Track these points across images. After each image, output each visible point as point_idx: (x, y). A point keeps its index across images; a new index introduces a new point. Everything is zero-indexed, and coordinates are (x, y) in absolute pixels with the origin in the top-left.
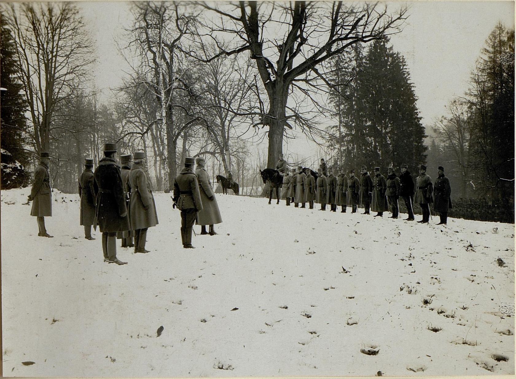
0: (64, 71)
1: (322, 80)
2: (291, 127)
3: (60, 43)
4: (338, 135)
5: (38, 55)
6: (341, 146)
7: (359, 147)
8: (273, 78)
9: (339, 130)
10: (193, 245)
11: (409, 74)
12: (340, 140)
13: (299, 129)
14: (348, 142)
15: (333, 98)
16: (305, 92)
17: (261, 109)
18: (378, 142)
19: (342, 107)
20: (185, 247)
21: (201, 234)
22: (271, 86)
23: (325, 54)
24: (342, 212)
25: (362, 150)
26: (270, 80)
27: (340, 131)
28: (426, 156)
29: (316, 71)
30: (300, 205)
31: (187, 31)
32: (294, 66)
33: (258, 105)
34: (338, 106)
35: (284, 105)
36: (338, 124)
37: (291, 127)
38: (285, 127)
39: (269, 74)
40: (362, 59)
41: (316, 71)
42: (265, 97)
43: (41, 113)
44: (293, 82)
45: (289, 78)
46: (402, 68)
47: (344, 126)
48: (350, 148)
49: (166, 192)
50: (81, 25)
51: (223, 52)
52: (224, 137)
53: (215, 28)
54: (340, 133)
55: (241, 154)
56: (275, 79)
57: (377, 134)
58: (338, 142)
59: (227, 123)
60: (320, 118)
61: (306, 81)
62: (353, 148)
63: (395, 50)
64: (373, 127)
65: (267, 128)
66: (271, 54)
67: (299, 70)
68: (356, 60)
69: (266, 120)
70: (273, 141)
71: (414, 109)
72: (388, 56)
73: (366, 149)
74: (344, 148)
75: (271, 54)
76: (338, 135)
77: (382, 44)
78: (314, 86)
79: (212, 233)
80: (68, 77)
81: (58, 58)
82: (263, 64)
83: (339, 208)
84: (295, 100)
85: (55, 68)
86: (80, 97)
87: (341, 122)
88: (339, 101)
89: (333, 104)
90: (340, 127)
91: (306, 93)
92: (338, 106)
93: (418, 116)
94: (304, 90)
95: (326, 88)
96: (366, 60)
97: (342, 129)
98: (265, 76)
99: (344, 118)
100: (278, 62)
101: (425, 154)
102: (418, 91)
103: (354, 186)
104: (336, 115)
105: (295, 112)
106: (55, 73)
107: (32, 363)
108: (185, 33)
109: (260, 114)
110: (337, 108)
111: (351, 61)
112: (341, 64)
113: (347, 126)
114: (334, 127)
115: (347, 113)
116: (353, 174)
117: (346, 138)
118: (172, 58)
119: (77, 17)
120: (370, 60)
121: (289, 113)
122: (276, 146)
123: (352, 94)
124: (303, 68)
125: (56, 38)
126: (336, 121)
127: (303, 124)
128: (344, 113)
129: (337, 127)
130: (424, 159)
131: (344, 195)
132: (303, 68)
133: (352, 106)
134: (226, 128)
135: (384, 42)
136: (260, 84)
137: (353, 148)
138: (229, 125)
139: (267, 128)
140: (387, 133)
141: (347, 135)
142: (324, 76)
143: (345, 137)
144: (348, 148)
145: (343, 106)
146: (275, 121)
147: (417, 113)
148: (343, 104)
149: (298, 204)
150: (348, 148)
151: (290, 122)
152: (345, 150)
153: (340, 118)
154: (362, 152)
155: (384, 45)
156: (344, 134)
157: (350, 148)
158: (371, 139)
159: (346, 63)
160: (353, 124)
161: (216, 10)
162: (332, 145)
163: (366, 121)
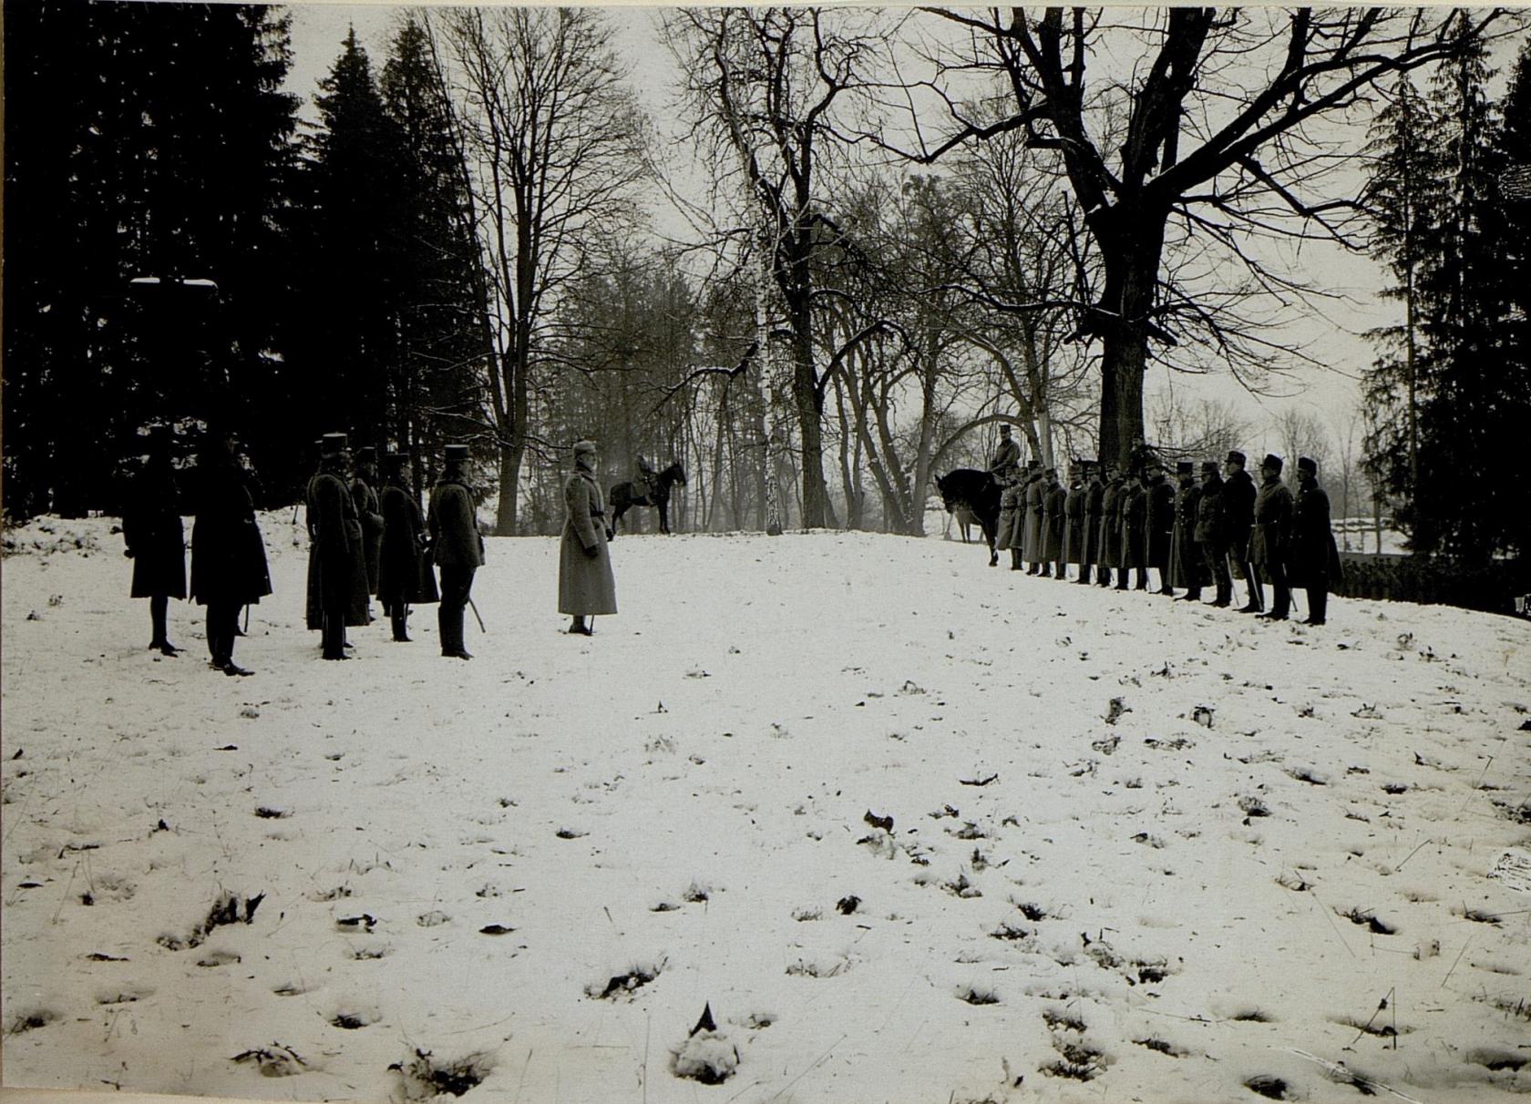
0: (561, 207)
1: (1275, 194)
3: (556, 130)
5: (495, 165)
10: (468, 648)
12: (1414, 371)
14: (1444, 377)
15: (1390, 240)
16: (1224, 234)
20: (446, 653)
21: (571, 631)
26: (1104, 202)
27: (1412, 345)
31: (851, 81)
36: (1404, 322)
38: (1151, 343)
41: (1255, 168)
43: (506, 320)
47: (1424, 327)
49: (770, 533)
50: (609, 76)
51: (971, 130)
53: (947, 59)
54: (1413, 352)
61: (1217, 201)
65: (1098, 347)
66: (1104, 125)
68: (1463, 116)
70: (1114, 381)
75: (1104, 125)
76: (1403, 356)
80: (576, 221)
81: (549, 173)
82: (1083, 163)
85: (542, 198)
86: (626, 272)
87: (1414, 318)
90: (1411, 332)
94: (1216, 227)
95: (725, 268)
97: (1421, 339)
104: (1399, 293)
106: (541, 210)
108: (844, 86)
111: (1445, 119)
114: (1390, 332)
115: (1435, 284)
116: (1137, 481)
118: (805, 159)
119: (595, 56)
122: (1122, 396)
124: (1209, 161)
125: (543, 116)
126: (1397, 312)
129: (1400, 330)
131: (1115, 541)
132: (1209, 161)
142: (1280, 180)
150: (1442, 397)
153: (1411, 303)
156: (1425, 353)
161: (940, 12)
162: (1386, 389)
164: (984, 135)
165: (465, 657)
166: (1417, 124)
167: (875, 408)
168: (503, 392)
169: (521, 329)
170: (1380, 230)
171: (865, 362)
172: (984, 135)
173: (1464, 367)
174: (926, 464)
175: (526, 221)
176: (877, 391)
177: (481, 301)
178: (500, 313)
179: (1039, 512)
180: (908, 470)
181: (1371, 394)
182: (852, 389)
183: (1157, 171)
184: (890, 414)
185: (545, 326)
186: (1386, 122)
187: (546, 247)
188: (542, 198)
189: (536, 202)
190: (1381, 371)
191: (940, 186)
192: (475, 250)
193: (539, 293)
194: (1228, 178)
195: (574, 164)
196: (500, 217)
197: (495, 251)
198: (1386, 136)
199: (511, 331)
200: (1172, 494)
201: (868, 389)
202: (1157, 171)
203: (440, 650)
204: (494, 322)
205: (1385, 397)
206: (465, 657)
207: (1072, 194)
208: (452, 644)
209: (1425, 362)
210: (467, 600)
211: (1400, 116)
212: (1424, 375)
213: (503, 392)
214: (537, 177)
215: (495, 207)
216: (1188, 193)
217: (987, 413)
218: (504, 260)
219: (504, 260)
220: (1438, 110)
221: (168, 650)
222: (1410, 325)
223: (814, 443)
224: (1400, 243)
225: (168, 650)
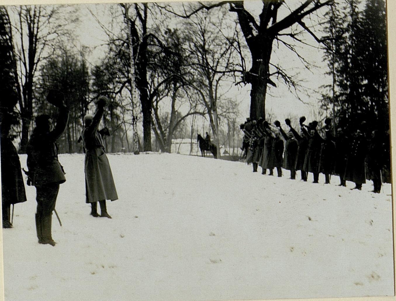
2: (274, 85)
4: (331, 95)
6: (335, 105)
7: (354, 108)
8: (255, 33)
12: (335, 100)
14: (343, 102)
17: (243, 67)
19: (336, 65)
22: (252, 43)
24: (314, 182)
27: (334, 91)
29: (303, 25)
30: (268, 171)
32: (279, 20)
37: (274, 85)
38: (268, 84)
40: (357, 13)
41: (303, 25)
42: (247, 53)
44: (279, 37)
47: (338, 85)
48: (345, 108)
52: (211, 97)
54: (334, 93)
55: (232, 114)
58: (331, 102)
59: (214, 83)
60: (304, 74)
61: (292, 35)
62: (348, 109)
68: (352, 15)
69: (247, 78)
70: (255, 100)
73: (361, 109)
74: (339, 108)
76: (331, 95)
79: (104, 214)
80: (50, 37)
83: (310, 176)
84: (280, 55)
85: (38, 28)
87: (335, 81)
88: (332, 59)
89: (327, 62)
90: (334, 86)
91: (292, 49)
92: (332, 64)
94: (290, 45)
96: (363, 15)
98: (247, 30)
99: (338, 76)
100: (261, 16)
104: (330, 74)
109: (242, 72)
110: (331, 66)
112: (335, 20)
113: (341, 85)
114: (327, 86)
115: (342, 71)
117: (341, 98)
121: (272, 70)
122: (258, 106)
123: (347, 52)
128: (337, 71)
129: (330, 86)
133: (347, 63)
136: (243, 41)
138: (217, 84)
139: (249, 86)
141: (341, 95)
144: (343, 108)
146: (258, 79)
148: (337, 62)
149: (265, 170)
150: (342, 108)
151: (273, 78)
152: (339, 110)
153: (334, 77)
157: (345, 108)
162: (325, 105)
163: (362, 80)
165: (53, 244)
166: (337, 18)
167: (154, 109)
168: (23, 99)
169: (30, 76)
173: (350, 99)
174: (172, 129)
175: (32, 36)
177: (14, 65)
178: (21, 70)
179: (269, 149)
180: (165, 130)
181: (321, 107)
184: (159, 110)
185: (37, 75)
186: (327, 16)
187: (39, 46)
188: (38, 28)
189: (35, 29)
191: (179, 32)
192: (12, 48)
193: (37, 63)
194: (296, 27)
195: (50, 16)
196: (22, 34)
197: (20, 47)
198: (326, 20)
199: (26, 77)
200: (160, 136)
203: (37, 239)
204: (19, 73)
205: (325, 108)
206: (53, 244)
208: (44, 235)
209: (338, 97)
210: (54, 209)
211: (331, 15)
212: (337, 101)
213: (23, 99)
214: (36, 21)
215: (20, 30)
217: (192, 111)
218: (23, 50)
219: (23, 50)
220: (344, 13)
222: (334, 85)
223: (148, 120)
224: (331, 57)
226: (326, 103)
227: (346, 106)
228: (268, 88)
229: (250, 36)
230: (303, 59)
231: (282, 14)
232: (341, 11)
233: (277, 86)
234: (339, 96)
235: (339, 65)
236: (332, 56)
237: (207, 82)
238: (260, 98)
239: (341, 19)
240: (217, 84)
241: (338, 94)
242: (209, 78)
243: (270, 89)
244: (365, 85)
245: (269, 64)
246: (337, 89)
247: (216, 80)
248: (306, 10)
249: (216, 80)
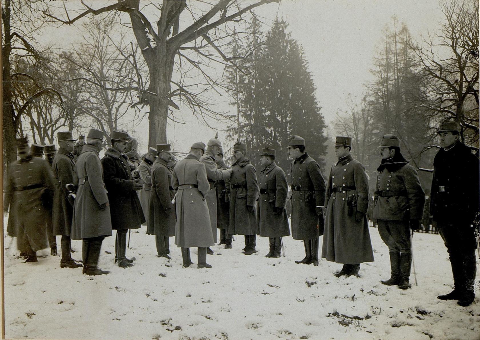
2: (177, 107)
4: (236, 125)
8: (153, 45)
9: (238, 120)
11: (307, 63)
13: (190, 111)
18: (279, 132)
19: (240, 95)
22: (150, 54)
23: (217, 17)
25: (261, 141)
26: (150, 46)
27: (238, 121)
28: (326, 147)
29: (208, 39)
33: (136, 79)
34: (236, 94)
35: (168, 80)
37: (177, 107)
38: (171, 107)
39: (149, 40)
41: (208, 39)
42: (145, 69)
44: (181, 51)
45: (173, 46)
46: (300, 55)
48: (249, 139)
54: (239, 124)
56: (155, 45)
57: (277, 125)
58: (236, 133)
59: (114, 111)
61: (195, 49)
62: (253, 139)
63: (293, 37)
64: (272, 116)
65: (147, 108)
67: (187, 35)
69: (145, 98)
71: (313, 98)
72: (287, 42)
76: (236, 125)
77: (281, 29)
78: (206, 56)
87: (239, 111)
90: (238, 117)
91: (196, 66)
92: (236, 94)
93: (318, 106)
94: (194, 62)
98: (143, 41)
100: (159, 23)
101: (325, 144)
102: (317, 80)
103: (274, 191)
104: (234, 103)
105: (179, 86)
107: (110, 253)
110: (235, 97)
113: (245, 115)
115: (246, 102)
117: (245, 129)
120: (269, 45)
121: (174, 87)
122: (158, 133)
123: (250, 82)
124: (192, 33)
126: (234, 110)
127: (193, 105)
129: (235, 116)
130: (325, 150)
132: (192, 33)
134: (113, 116)
135: (282, 28)
137: (253, 139)
138: (117, 112)
139: (147, 108)
140: (287, 123)
141: (246, 125)
143: (244, 127)
145: (241, 94)
147: (316, 102)
148: (242, 92)
150: (247, 139)
151: (175, 99)
153: (238, 107)
154: (262, 143)
155: (283, 31)
158: (270, 130)
159: (244, 49)
160: (253, 114)
162: (230, 136)
164: (96, 13)
170: (228, 82)
171: (44, 121)
172: (96, 13)
176: (50, 132)
181: (226, 138)
182: (39, 132)
183: (171, 36)
186: (230, 46)
190: (229, 130)
194: (200, 40)
201: (46, 131)
202: (171, 36)
207: (135, 41)
211: (234, 44)
216: (183, 46)
221: (160, 275)
222: (238, 115)
225: (160, 275)
226: (231, 133)
227: (432, 76)
228: (169, 112)
229: (147, 47)
230: (210, 78)
231: (185, 21)
232: (243, 40)
233: (179, 106)
234: (244, 127)
235: (243, 95)
236: (236, 86)
237: (106, 111)
238: (160, 123)
239: (244, 49)
240: (117, 112)
241: (242, 124)
242: (108, 107)
243: (173, 114)
244: (268, 116)
245: (171, 83)
246: (243, 120)
247: (116, 108)
248: (211, 21)
249: (116, 108)
